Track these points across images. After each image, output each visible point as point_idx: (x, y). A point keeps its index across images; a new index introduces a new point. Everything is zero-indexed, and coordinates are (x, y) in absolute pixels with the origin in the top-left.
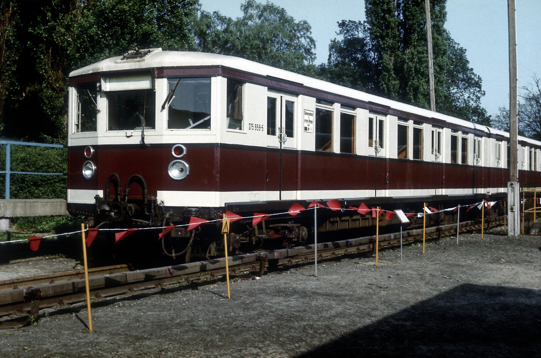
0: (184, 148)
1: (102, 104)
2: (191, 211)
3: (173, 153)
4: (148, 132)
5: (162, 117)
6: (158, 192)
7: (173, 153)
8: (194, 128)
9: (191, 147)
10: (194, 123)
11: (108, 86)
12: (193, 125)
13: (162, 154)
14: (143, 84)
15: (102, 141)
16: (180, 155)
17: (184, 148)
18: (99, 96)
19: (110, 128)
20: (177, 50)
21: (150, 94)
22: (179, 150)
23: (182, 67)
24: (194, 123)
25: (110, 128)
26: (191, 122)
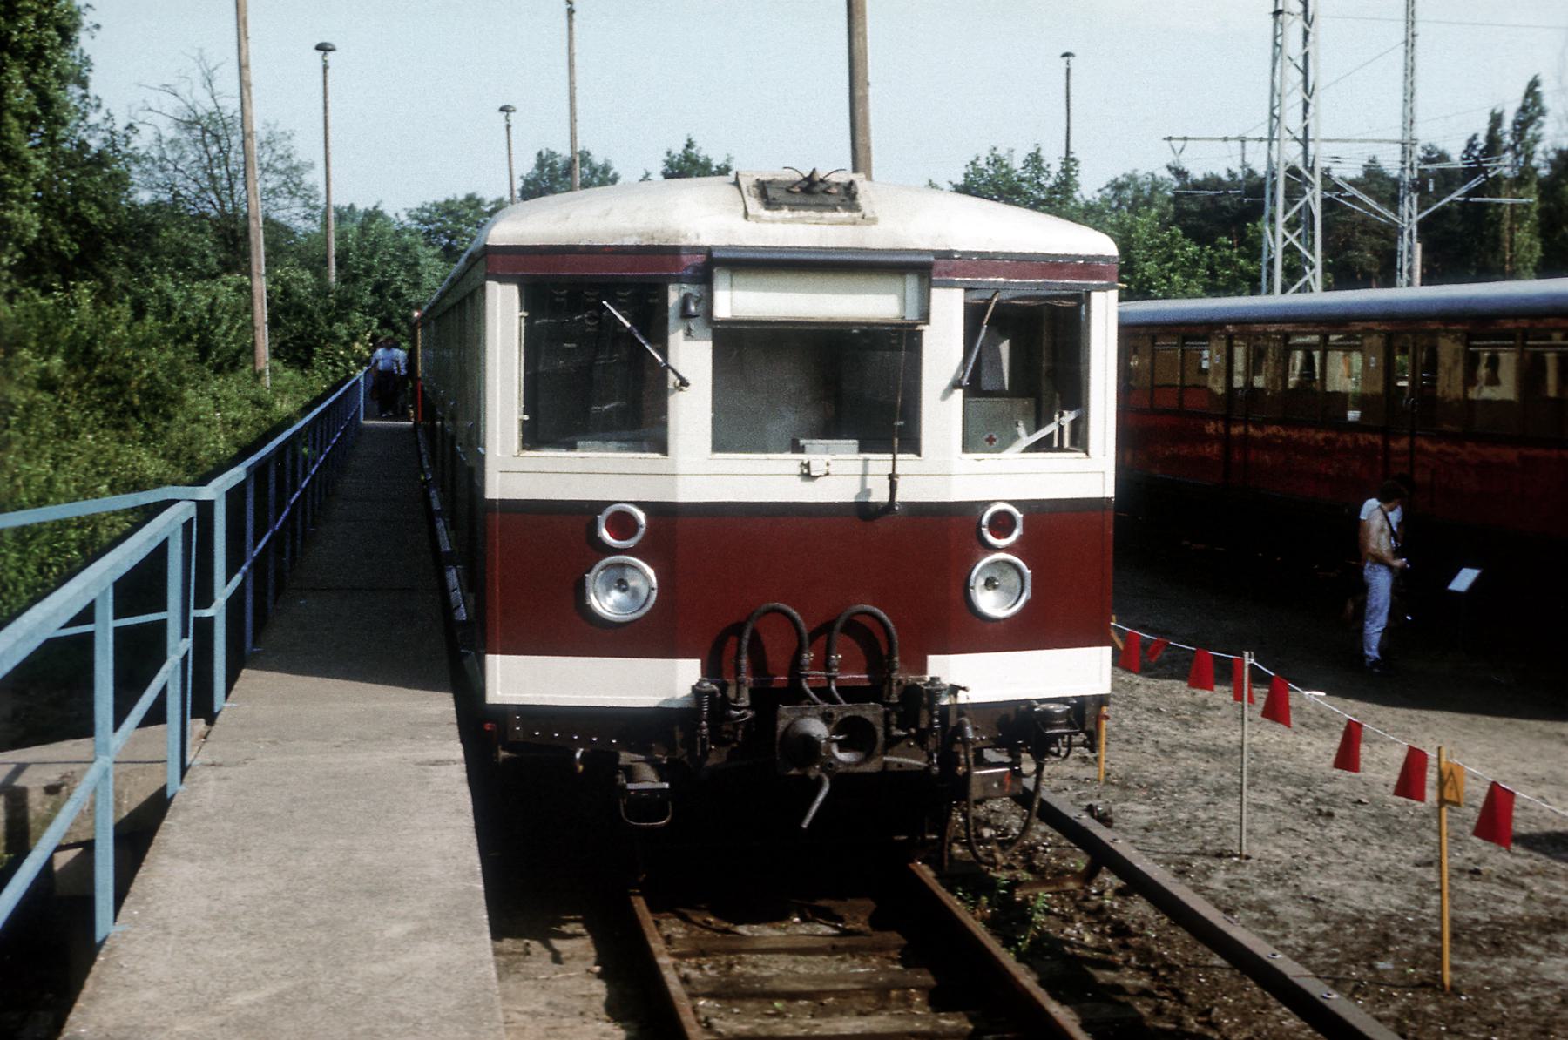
0: (641, 516)
1: (691, 357)
2: (1047, 718)
3: (605, 534)
4: (905, 461)
5: (941, 413)
6: (698, 662)
7: (605, 534)
8: (1029, 449)
9: (1037, 511)
10: (1029, 434)
11: (735, 301)
12: (1027, 440)
13: (951, 531)
14: (875, 304)
15: (690, 491)
16: (998, 537)
17: (641, 516)
18: (681, 333)
19: (719, 446)
20: (1018, 205)
21: (903, 340)
22: (622, 524)
23: (983, 255)
24: (1029, 434)
25: (719, 446)
26: (1021, 430)
